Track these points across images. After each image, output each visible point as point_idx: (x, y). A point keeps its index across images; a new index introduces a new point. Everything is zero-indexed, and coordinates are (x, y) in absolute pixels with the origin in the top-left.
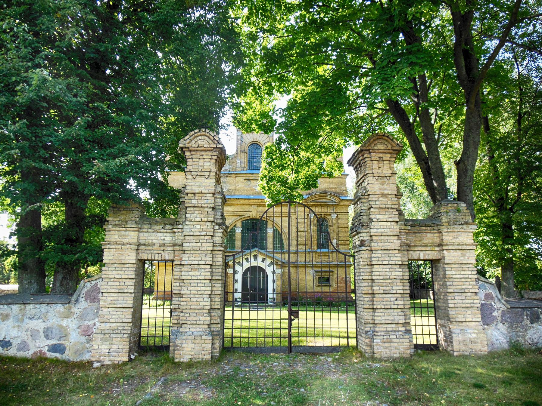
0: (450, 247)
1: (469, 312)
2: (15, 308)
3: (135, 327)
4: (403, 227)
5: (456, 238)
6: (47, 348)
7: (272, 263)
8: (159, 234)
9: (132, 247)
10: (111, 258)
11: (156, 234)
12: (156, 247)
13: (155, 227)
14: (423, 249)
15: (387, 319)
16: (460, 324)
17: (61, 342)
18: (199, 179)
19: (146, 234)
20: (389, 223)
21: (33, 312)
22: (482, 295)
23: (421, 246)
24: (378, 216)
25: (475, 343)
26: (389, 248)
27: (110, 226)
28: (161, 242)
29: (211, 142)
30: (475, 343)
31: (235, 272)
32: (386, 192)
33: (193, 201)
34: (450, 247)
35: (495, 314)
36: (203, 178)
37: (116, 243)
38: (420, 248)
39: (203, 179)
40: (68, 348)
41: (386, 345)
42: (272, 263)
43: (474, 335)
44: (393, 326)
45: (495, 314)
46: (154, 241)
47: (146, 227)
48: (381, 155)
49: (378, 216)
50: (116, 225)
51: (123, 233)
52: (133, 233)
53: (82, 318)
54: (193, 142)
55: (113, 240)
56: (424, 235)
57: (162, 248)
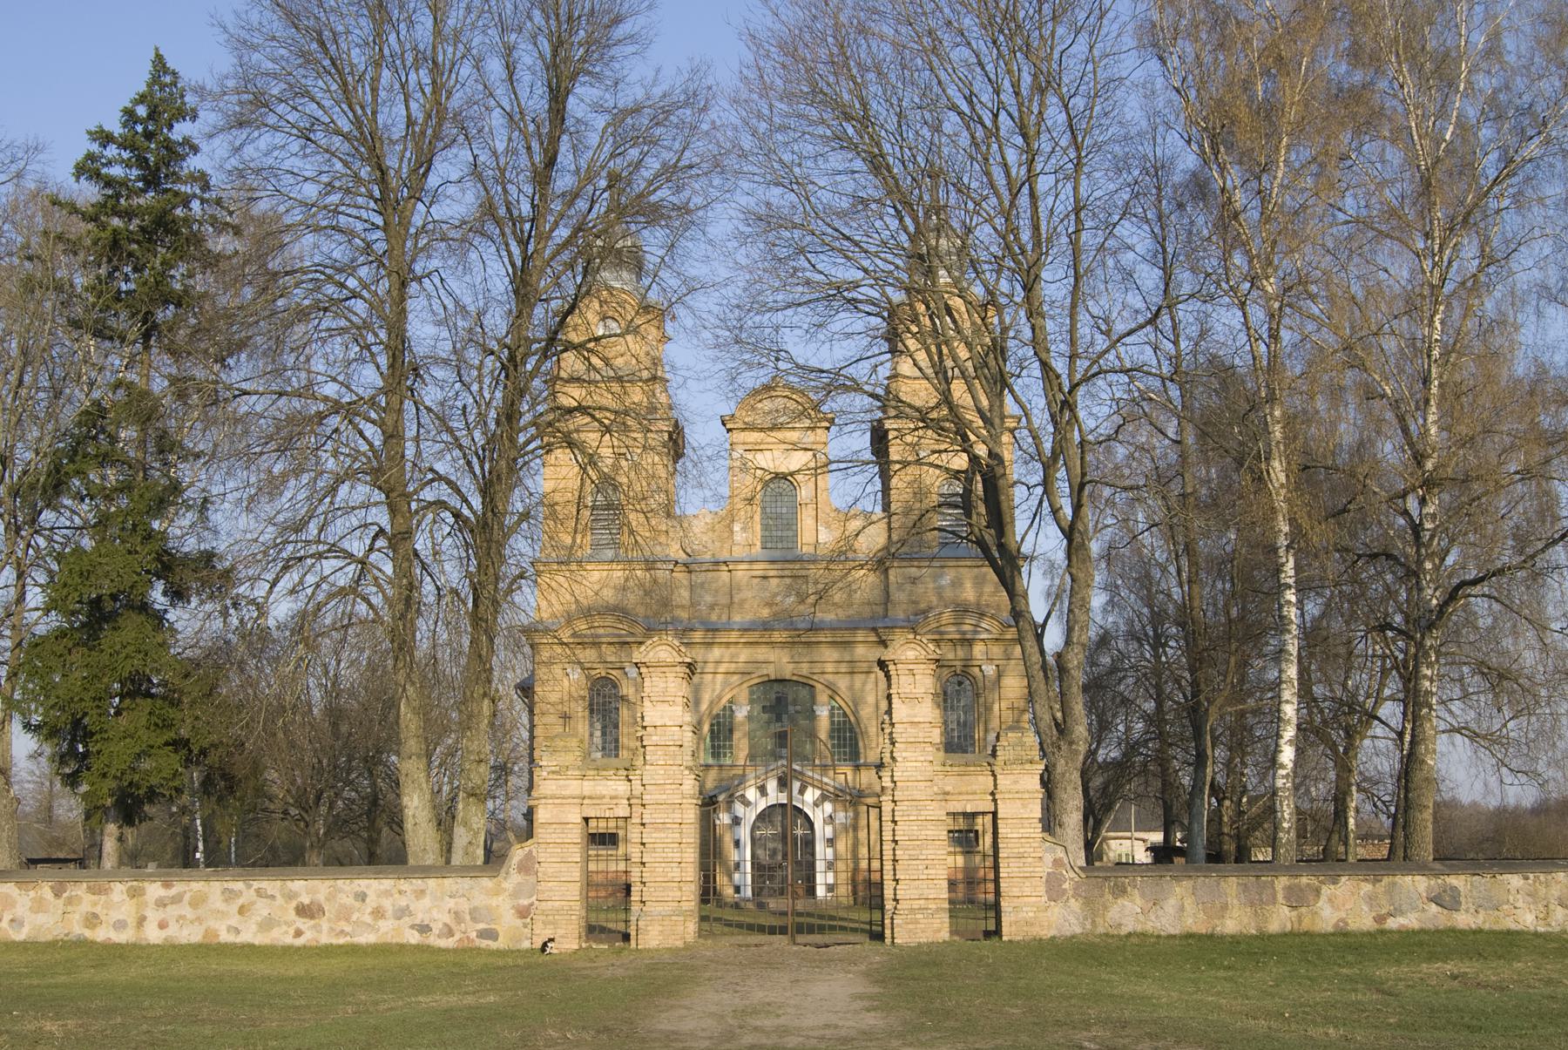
0: (1007, 796)
1: (1027, 884)
2: (432, 883)
3: (1194, 549)
4: (940, 768)
5: (1016, 782)
6: (475, 934)
7: (824, 798)
8: (609, 783)
9: (575, 801)
10: (548, 816)
11: (605, 782)
12: (606, 800)
13: (604, 773)
14: (970, 797)
15: (914, 893)
16: (1016, 900)
17: (493, 926)
18: (661, 707)
19: (592, 783)
20: (919, 764)
21: (454, 888)
22: (1049, 858)
23: (967, 794)
24: (904, 754)
25: (1032, 925)
26: (918, 798)
27: (545, 774)
28: (613, 793)
29: (675, 654)
30: (1032, 925)
31: (736, 821)
32: (916, 720)
33: (654, 738)
34: (1007, 796)
35: (1066, 886)
36: (666, 704)
37: (553, 797)
38: (965, 797)
39: (665, 707)
40: (501, 934)
41: (911, 926)
42: (824, 798)
43: (1031, 914)
44: (922, 902)
45: (1066, 886)
46: (604, 792)
47: (592, 773)
48: (911, 667)
49: (904, 754)
50: (553, 772)
51: (562, 782)
52: (575, 782)
53: (515, 894)
54: (651, 654)
55: (549, 792)
56: (973, 778)
57: (615, 801)
